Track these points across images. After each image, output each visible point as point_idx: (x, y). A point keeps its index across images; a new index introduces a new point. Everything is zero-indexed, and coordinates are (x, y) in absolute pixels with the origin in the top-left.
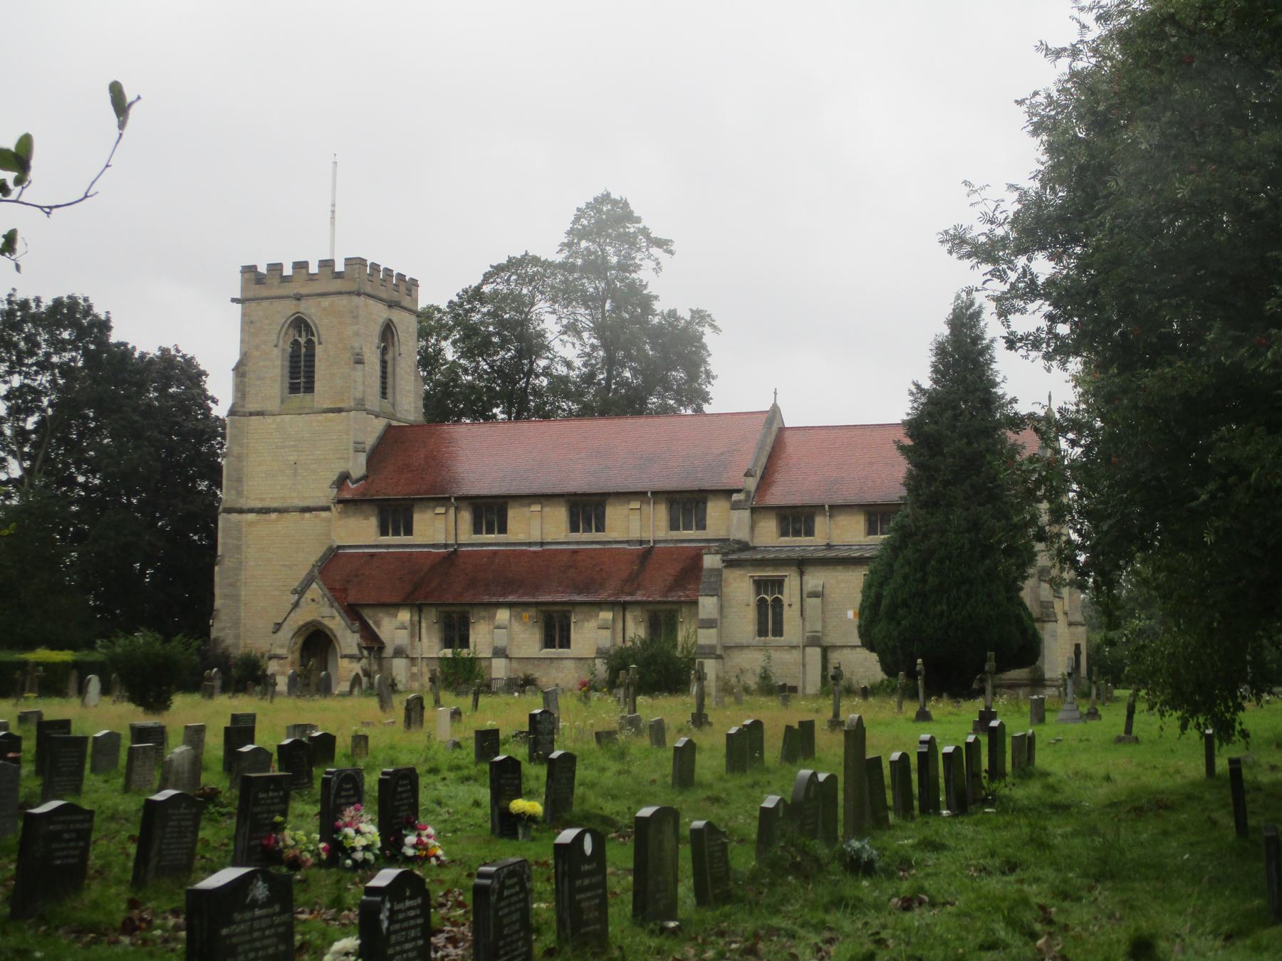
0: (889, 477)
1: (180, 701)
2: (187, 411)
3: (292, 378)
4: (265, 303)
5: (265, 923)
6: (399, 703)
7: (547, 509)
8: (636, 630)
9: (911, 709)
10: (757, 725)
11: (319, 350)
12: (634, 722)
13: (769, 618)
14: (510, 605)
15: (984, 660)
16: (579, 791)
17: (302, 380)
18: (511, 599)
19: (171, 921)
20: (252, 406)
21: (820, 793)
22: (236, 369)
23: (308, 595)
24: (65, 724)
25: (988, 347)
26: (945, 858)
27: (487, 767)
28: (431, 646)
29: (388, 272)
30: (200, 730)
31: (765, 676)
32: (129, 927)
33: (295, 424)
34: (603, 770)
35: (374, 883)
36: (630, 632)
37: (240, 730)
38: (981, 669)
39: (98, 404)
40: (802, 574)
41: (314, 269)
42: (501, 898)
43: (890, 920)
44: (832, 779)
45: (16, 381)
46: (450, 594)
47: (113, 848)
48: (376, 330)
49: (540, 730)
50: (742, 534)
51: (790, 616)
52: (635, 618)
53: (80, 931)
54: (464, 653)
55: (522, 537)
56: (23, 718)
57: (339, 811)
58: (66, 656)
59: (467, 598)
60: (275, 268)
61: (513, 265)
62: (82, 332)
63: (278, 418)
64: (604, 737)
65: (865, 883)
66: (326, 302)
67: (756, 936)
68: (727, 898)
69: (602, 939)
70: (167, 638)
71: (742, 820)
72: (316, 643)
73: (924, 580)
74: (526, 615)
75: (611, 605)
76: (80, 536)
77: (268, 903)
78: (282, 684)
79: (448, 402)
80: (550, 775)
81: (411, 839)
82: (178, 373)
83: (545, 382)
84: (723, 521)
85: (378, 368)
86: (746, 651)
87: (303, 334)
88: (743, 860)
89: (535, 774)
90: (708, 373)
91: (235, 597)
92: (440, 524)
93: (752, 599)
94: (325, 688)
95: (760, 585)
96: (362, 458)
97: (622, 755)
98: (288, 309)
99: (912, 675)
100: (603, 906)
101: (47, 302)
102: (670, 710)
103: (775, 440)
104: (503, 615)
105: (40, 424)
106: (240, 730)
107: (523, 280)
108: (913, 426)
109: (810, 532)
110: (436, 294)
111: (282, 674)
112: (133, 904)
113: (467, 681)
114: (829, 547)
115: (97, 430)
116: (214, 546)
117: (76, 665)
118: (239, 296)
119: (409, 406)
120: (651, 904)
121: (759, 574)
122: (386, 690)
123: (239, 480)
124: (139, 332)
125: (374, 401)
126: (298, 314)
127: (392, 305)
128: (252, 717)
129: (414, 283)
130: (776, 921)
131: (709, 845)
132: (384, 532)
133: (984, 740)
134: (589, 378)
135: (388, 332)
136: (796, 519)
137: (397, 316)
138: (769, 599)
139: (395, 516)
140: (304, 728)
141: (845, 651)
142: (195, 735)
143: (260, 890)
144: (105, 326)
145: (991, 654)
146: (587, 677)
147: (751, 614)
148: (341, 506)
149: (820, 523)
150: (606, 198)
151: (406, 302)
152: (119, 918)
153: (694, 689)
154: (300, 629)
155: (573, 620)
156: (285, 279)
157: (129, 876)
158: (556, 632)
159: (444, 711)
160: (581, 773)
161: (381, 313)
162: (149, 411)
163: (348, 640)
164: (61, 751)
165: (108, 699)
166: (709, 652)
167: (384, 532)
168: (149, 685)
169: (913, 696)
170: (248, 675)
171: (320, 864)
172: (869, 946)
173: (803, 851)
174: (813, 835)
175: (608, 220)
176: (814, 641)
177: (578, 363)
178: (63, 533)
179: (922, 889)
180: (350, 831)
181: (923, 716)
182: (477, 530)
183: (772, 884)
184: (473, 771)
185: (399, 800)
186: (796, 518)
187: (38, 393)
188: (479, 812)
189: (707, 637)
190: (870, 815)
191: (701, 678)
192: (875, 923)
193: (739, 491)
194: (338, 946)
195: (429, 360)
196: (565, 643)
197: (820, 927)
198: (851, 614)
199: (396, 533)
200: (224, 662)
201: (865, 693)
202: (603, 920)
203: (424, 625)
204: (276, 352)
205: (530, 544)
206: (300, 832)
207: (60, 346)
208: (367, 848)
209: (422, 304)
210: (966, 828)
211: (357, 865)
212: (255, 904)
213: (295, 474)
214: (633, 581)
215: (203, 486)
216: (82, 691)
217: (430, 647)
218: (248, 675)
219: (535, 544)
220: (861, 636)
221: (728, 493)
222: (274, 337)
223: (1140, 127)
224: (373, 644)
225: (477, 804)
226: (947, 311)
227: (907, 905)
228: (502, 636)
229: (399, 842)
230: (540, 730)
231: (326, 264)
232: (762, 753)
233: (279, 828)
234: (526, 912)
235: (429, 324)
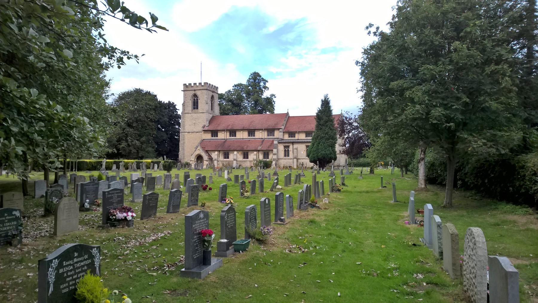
0: (312, 126)
5: (203, 223)
10: (290, 174)
13: (287, 153)
14: (237, 151)
20: (186, 112)
29: (212, 85)
33: (195, 115)
37: (187, 176)
41: (198, 84)
44: (310, 186)
48: (210, 97)
50: (282, 137)
51: (291, 153)
55: (239, 138)
60: (190, 84)
72: (199, 158)
77: (203, 219)
82: (171, 106)
91: (184, 149)
92: (223, 135)
95: (285, 147)
96: (208, 122)
98: (193, 92)
104: (235, 153)
106: (187, 176)
116: (179, 139)
123: (184, 127)
124: (163, 98)
127: (213, 92)
129: (217, 88)
135: (212, 97)
136: (292, 134)
137: (214, 94)
139: (214, 133)
142: (177, 176)
147: (283, 152)
149: (297, 135)
156: (192, 87)
158: (246, 156)
161: (211, 94)
163: (205, 157)
167: (212, 136)
182: (230, 136)
196: (248, 158)
212: (200, 219)
215: (177, 127)
218: (188, 165)
221: (279, 129)
224: (211, 159)
228: (235, 157)
231: (200, 84)
235: (221, 96)
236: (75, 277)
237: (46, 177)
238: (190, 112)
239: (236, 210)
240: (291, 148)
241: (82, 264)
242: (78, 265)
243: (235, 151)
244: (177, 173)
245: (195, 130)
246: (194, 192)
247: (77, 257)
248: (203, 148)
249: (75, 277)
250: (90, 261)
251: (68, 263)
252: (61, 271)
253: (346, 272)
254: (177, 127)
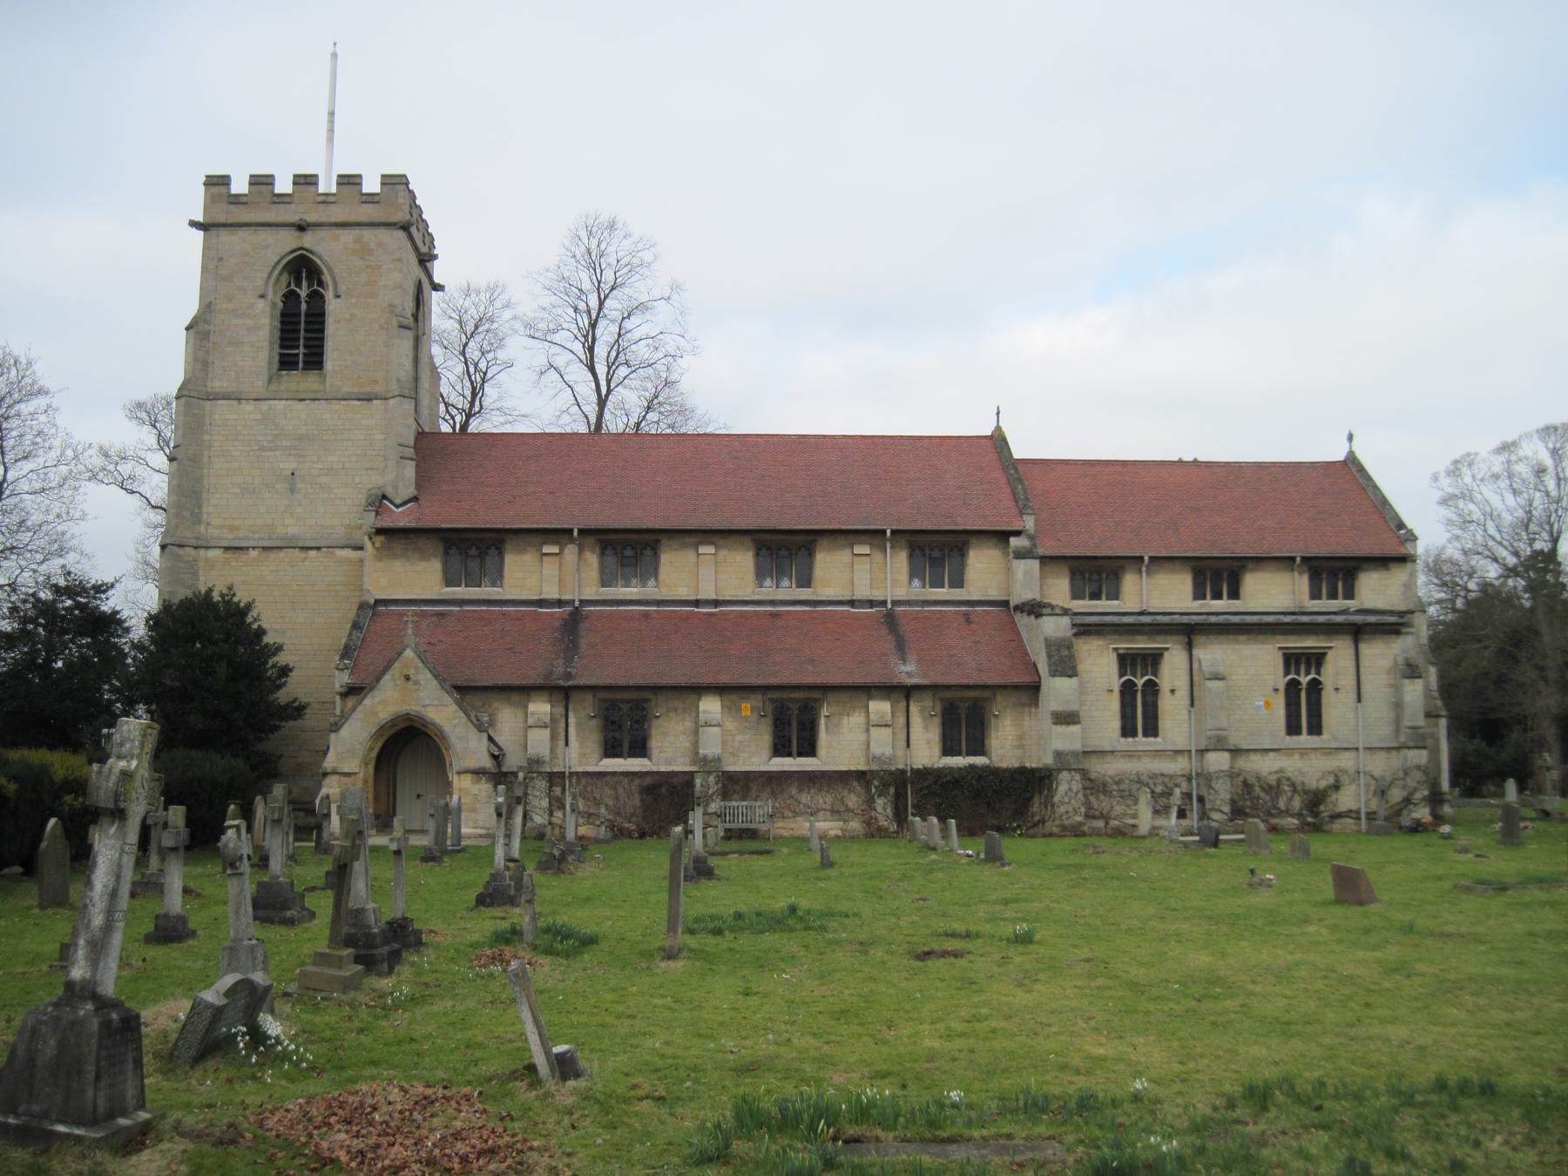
3: (282, 347)
4: (244, 233)
7: (723, 553)
11: (333, 307)
13: (1140, 710)
14: (721, 690)
17: (302, 350)
20: (218, 385)
33: (294, 415)
40: (1190, 647)
51: (1172, 708)
52: (922, 711)
55: (683, 593)
63: (264, 406)
66: (347, 236)
74: (746, 707)
86: (1109, 758)
87: (305, 283)
93: (1116, 683)
95: (1127, 661)
96: (410, 470)
98: (283, 244)
109: (1115, 595)
118: (200, 218)
121: (1124, 645)
141: (1253, 757)
147: (1114, 704)
148: (379, 540)
149: (1130, 582)
154: (382, 728)
155: (824, 712)
193: (1017, 533)
203: (572, 720)
204: (261, 305)
205: (697, 603)
213: (293, 490)
217: (582, 755)
219: (707, 603)
222: (260, 283)
231: (305, 181)
238: (260, 385)
240: (1173, 668)
243: (700, 690)
245: (291, 528)
253: (361, 1031)
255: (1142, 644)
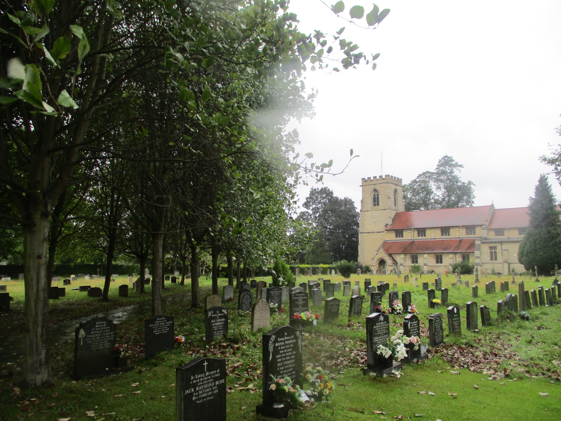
0: (526, 222)
1: (352, 275)
2: (351, 211)
6: (402, 276)
8: (459, 259)
9: (534, 279)
10: (493, 283)
12: (460, 282)
13: (493, 256)
14: (428, 253)
15: (555, 266)
16: (449, 297)
18: (427, 252)
19: (358, 325)
21: (513, 300)
22: (362, 201)
23: (380, 252)
24: (329, 281)
25: (550, 187)
26: (548, 317)
27: (426, 292)
28: (409, 263)
30: (358, 282)
31: (493, 271)
32: (349, 326)
34: (454, 293)
35: (406, 317)
36: (457, 260)
37: (367, 283)
38: (553, 269)
39: (331, 210)
41: (378, 178)
42: (435, 322)
43: (535, 332)
44: (516, 296)
45: (314, 206)
46: (412, 251)
47: (344, 308)
48: (393, 191)
49: (438, 283)
51: (499, 255)
53: (339, 326)
54: (417, 265)
55: (429, 238)
56: (319, 279)
57: (393, 300)
58: (327, 266)
59: (417, 252)
60: (369, 178)
61: (424, 174)
62: (328, 195)
64: (453, 285)
65: (527, 322)
67: (499, 334)
68: (490, 325)
69: (460, 332)
70: (349, 261)
71: (493, 306)
72: (382, 262)
73: (535, 246)
75: (453, 253)
76: (329, 239)
78: (375, 272)
79: (410, 207)
80: (442, 294)
81: (410, 308)
82: (348, 202)
83: (433, 201)
84: (480, 233)
85: (394, 199)
88: (494, 315)
89: (438, 293)
90: (474, 196)
94: (384, 273)
95: (491, 248)
96: (391, 220)
97: (458, 289)
98: (372, 187)
99: (534, 270)
100: (459, 325)
101: (320, 189)
102: (469, 278)
103: (492, 211)
104: (426, 256)
105: (319, 216)
106: (367, 283)
107: (426, 177)
108: (530, 208)
109: (503, 235)
110: (406, 182)
111: (374, 268)
112: (349, 321)
113: (418, 271)
114: (509, 238)
115: (331, 216)
116: (358, 241)
117: (329, 268)
119: (401, 208)
120: (471, 325)
121: (490, 245)
122: (399, 273)
124: (340, 193)
125: (393, 207)
126: (375, 189)
127: (396, 185)
128: (370, 279)
130: (504, 331)
131: (485, 312)
132: (397, 237)
133: (556, 287)
134: (444, 200)
135: (395, 191)
137: (397, 187)
138: (493, 251)
139: (399, 233)
140: (381, 282)
142: (357, 283)
143: (382, 318)
144: (332, 193)
145: (556, 265)
146: (447, 271)
149: (506, 232)
150: (446, 156)
151: (399, 184)
152: (347, 323)
153: (475, 273)
156: (371, 181)
157: (348, 314)
158: (439, 259)
159: (414, 278)
160: (449, 293)
161: (394, 187)
162: (342, 211)
163: (389, 261)
164: (329, 287)
165: (336, 275)
166: (478, 264)
168: (346, 272)
169: (534, 275)
170: (366, 270)
171: (389, 313)
172: (531, 338)
173: (510, 314)
174: (512, 310)
175: (447, 161)
176: (506, 262)
177: (441, 196)
178: (325, 239)
179: (543, 325)
180: (396, 306)
181: (537, 281)
182: (419, 236)
183: (502, 322)
184: (422, 292)
185: (407, 298)
186: (499, 232)
187: (318, 208)
188: (425, 302)
189: (477, 261)
190: (526, 305)
191: (477, 271)
192: (531, 333)
194: (398, 332)
195: (405, 197)
196: (441, 262)
197: (516, 333)
198: (515, 255)
199: (399, 237)
200: (361, 267)
201: (521, 275)
202: (460, 328)
206: (384, 305)
207: (323, 198)
208: (400, 310)
209: (403, 184)
210: (553, 309)
211: (398, 314)
212: (381, 321)
214: (458, 247)
216: (331, 273)
218: (366, 270)
220: (519, 260)
221: (481, 225)
223: (256, 197)
224: (395, 262)
225: (424, 300)
226: (538, 178)
227: (539, 328)
228: (426, 260)
229: (407, 309)
230: (438, 283)
231: (381, 177)
232: (495, 288)
233: (379, 304)
234: (441, 326)
235: (405, 189)
236: (285, 351)
237: (231, 283)
239: (419, 317)
240: (499, 250)
241: (290, 342)
242: (287, 342)
244: (357, 280)
246: (375, 298)
247: (287, 336)
248: (387, 251)
249: (285, 351)
250: (295, 341)
251: (281, 339)
252: (277, 344)
254: (355, 227)
255: (493, 245)
